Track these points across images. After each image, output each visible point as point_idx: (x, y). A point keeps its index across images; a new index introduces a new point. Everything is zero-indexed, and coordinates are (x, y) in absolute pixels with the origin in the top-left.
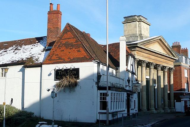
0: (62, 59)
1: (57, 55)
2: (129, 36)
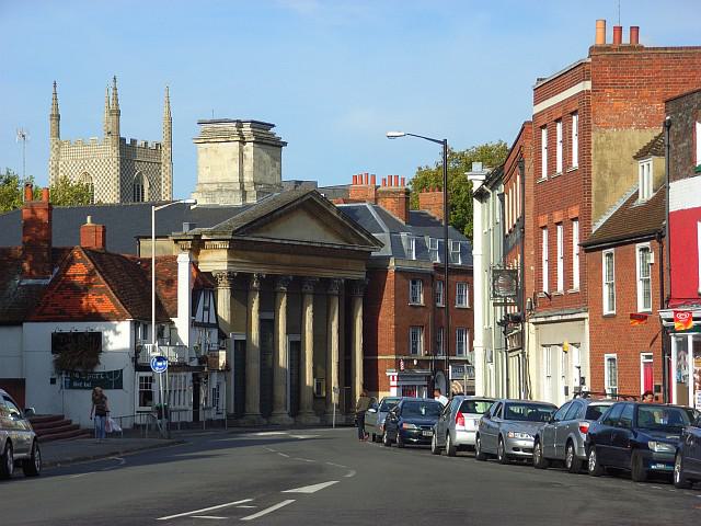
0: (65, 314)
1: (56, 305)
2: (215, 187)
